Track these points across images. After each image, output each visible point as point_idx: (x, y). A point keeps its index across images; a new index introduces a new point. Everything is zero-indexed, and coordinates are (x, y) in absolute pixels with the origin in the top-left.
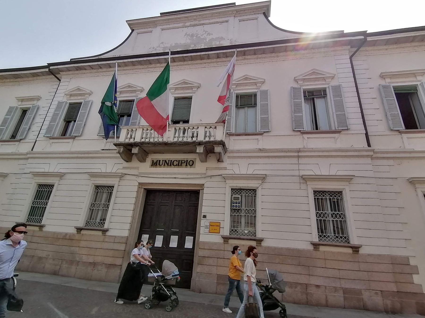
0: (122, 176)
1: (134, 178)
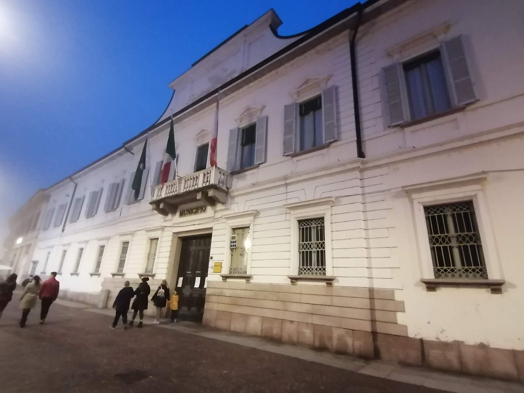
0: (163, 228)
1: (170, 229)
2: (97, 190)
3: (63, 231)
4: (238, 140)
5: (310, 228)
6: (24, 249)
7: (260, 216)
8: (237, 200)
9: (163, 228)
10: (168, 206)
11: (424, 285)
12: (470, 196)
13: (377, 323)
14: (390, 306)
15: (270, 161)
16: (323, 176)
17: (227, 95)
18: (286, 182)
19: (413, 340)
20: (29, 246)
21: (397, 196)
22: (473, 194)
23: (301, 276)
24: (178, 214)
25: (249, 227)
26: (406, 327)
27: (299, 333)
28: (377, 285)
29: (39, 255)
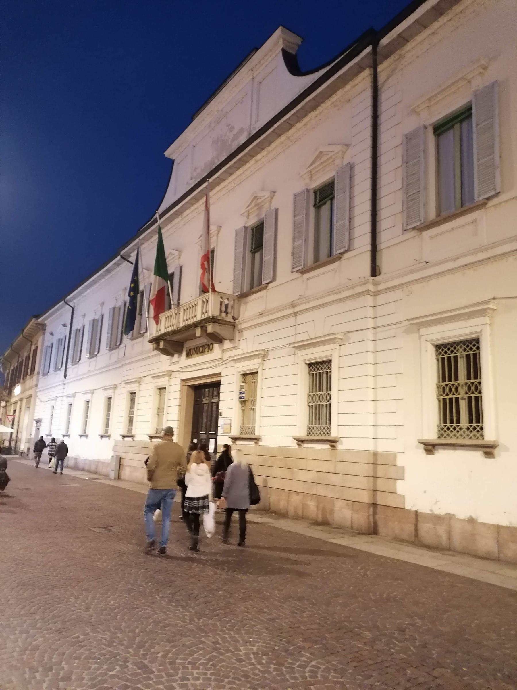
0: (169, 374)
2: (97, 317)
3: (65, 376)
4: (245, 245)
5: (456, 358)
6: (25, 401)
7: (270, 357)
8: (246, 334)
9: (169, 374)
10: (172, 344)
11: (423, 446)
12: (476, 333)
13: (379, 493)
14: (391, 472)
15: (280, 279)
16: (333, 302)
17: (270, 143)
18: (294, 310)
19: (409, 511)
20: (29, 397)
21: (408, 331)
22: (478, 329)
23: (309, 437)
24: (184, 354)
25: (257, 373)
26: (403, 497)
27: (305, 506)
28: (383, 447)
29: (41, 409)
